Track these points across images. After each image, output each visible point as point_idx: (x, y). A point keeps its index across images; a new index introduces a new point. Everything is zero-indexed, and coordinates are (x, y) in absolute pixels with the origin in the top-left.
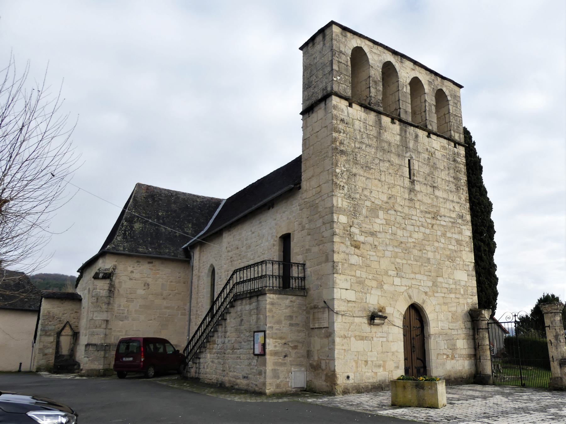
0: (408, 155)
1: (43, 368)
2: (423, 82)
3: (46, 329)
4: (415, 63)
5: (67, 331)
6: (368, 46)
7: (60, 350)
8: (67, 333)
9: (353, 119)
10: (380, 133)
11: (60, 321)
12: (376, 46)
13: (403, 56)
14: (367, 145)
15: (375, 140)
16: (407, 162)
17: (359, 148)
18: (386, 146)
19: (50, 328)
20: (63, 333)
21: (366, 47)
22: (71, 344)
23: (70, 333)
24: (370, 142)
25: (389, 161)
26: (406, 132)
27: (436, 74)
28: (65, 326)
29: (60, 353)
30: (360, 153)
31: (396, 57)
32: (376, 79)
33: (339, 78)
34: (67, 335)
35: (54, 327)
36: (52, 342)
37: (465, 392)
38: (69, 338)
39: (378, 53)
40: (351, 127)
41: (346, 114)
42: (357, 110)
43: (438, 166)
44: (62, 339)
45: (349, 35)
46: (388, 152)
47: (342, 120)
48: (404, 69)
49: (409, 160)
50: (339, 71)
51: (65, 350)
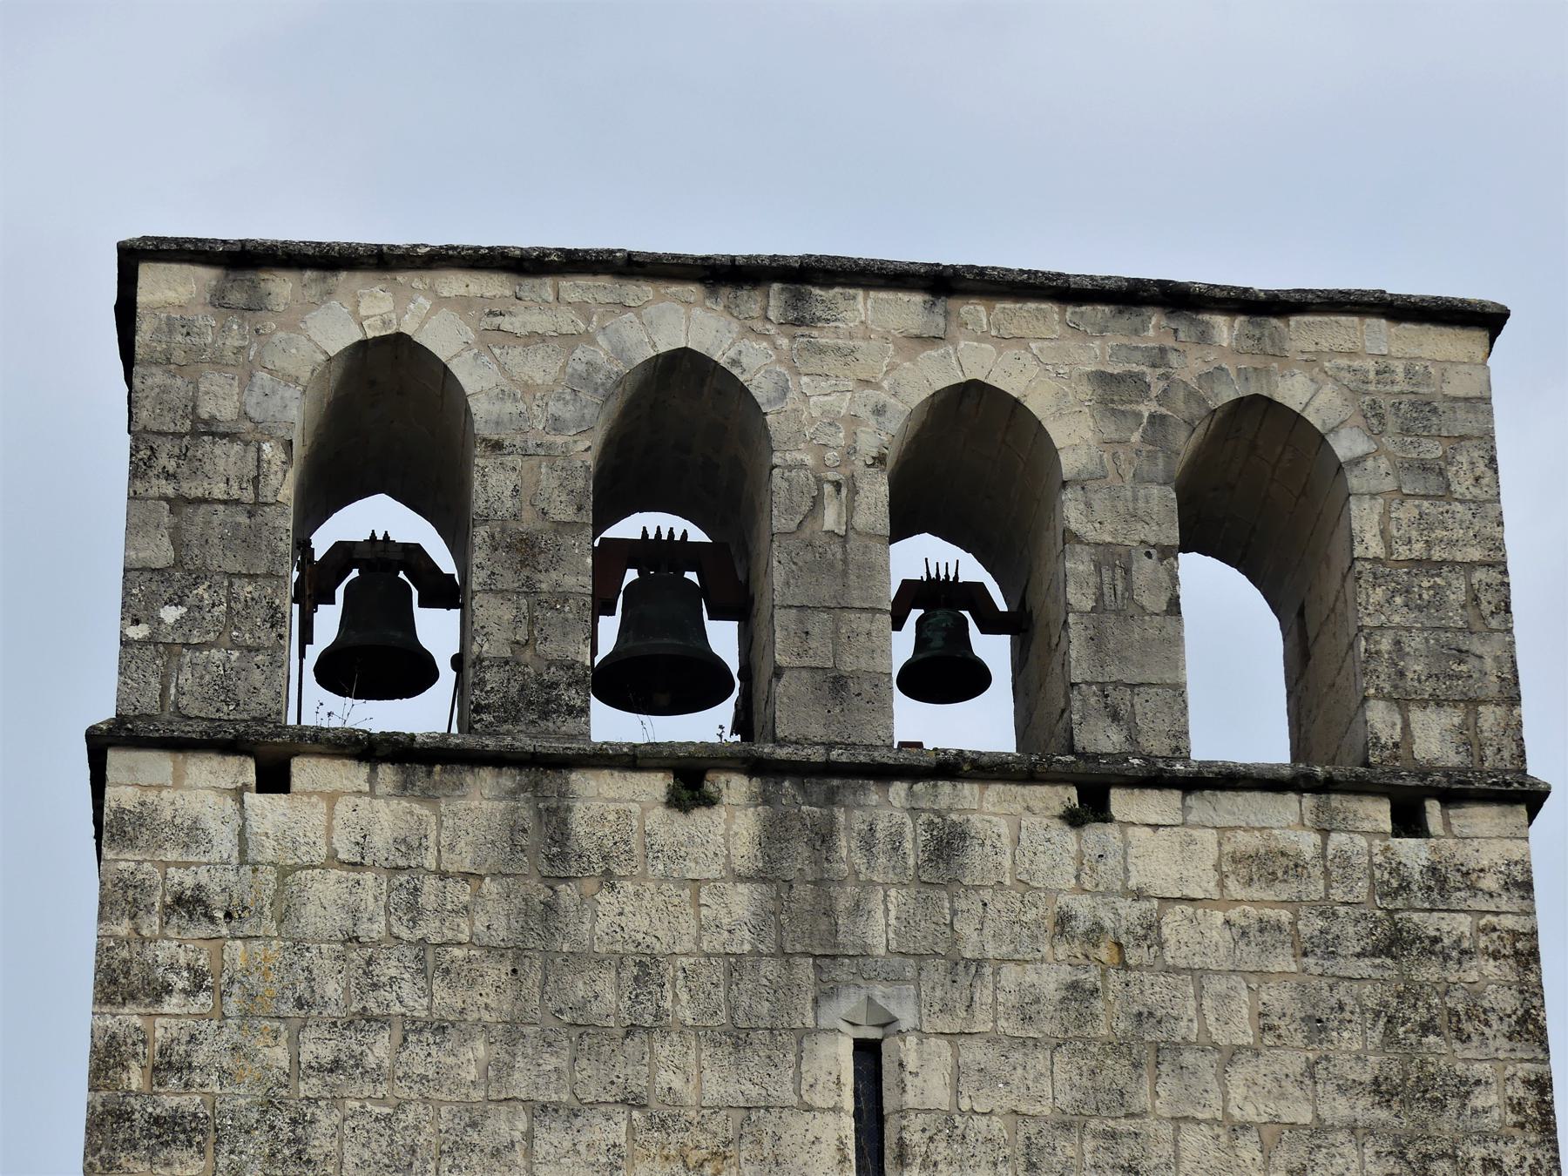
0: (848, 1004)
2: (1036, 405)
4: (942, 283)
6: (463, 304)
9: (284, 872)
10: (550, 907)
12: (545, 287)
13: (805, 277)
14: (413, 1027)
15: (497, 972)
16: (836, 1059)
17: (336, 1066)
18: (607, 995)
21: (433, 318)
24: (445, 998)
25: (633, 1102)
26: (824, 838)
27: (1179, 300)
30: (336, 1101)
31: (751, 302)
32: (529, 522)
33: (170, 614)
39: (566, 321)
40: (271, 927)
41: (225, 846)
42: (332, 798)
43: (1186, 1029)
45: (282, 286)
46: (630, 1031)
47: (189, 904)
48: (831, 363)
49: (868, 1053)
50: (179, 563)
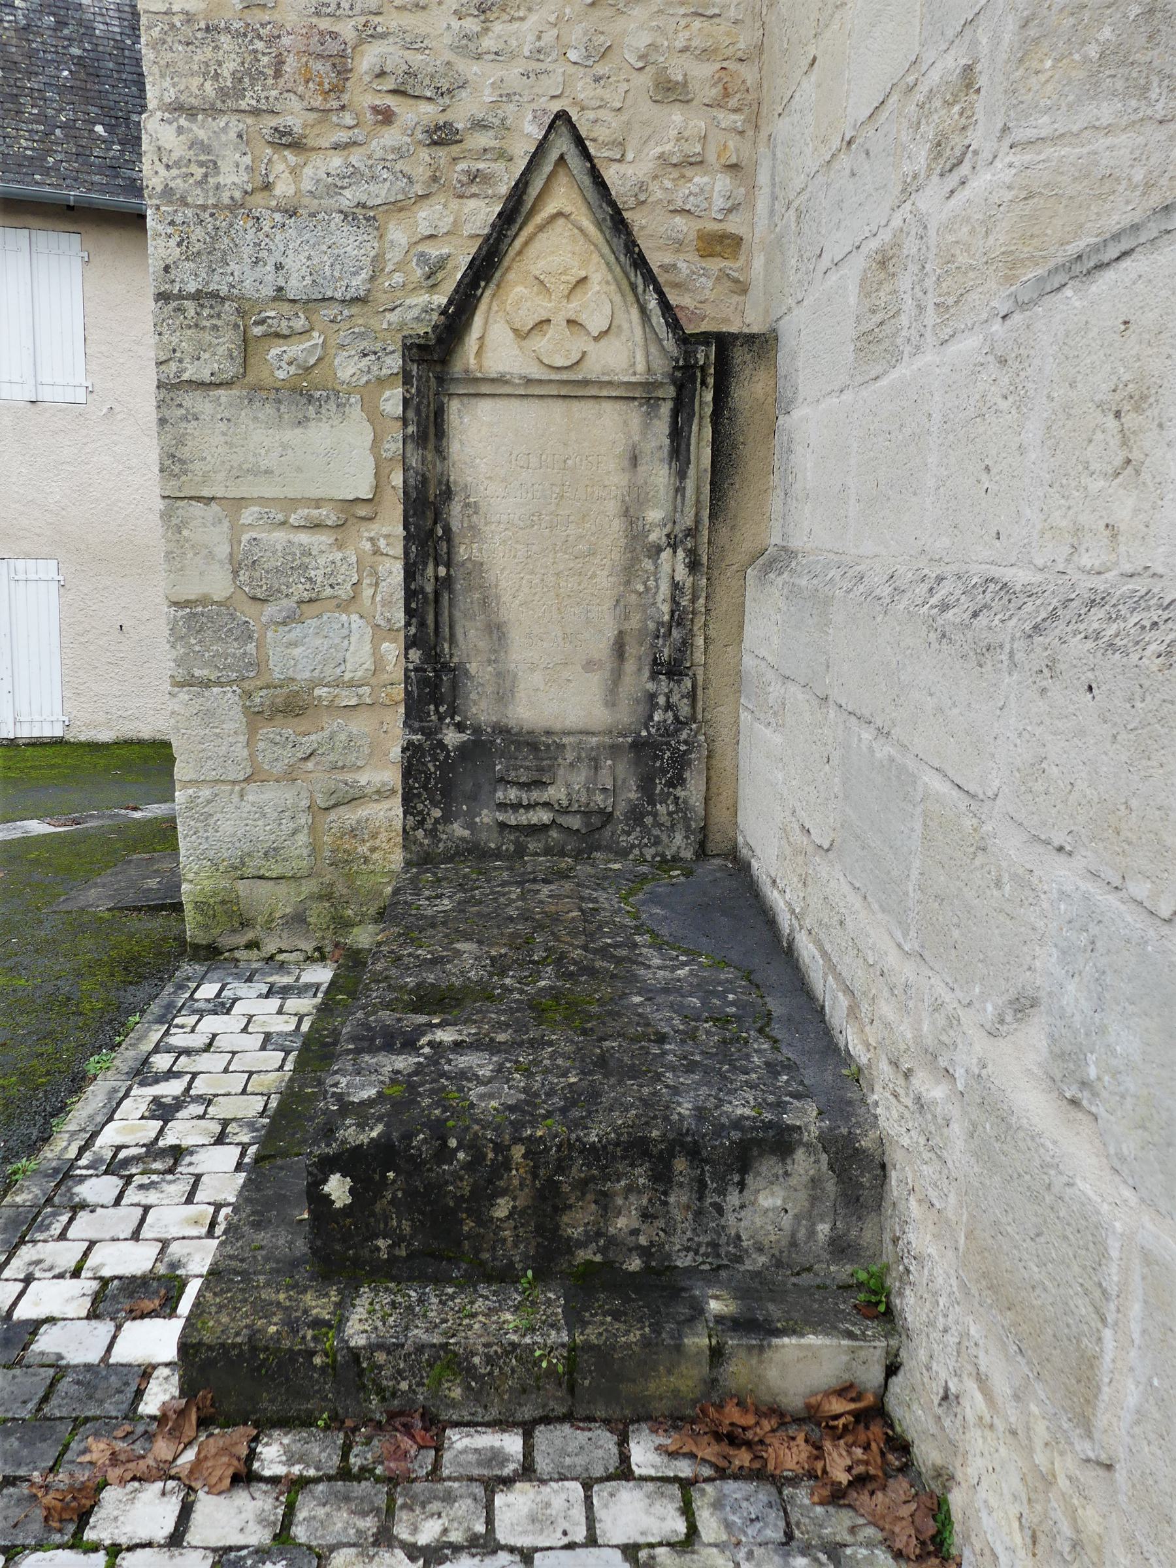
1: (278, 899)
3: (248, 277)
5: (561, 306)
7: (469, 644)
8: (556, 347)
11: (442, 136)
19: (301, 258)
20: (492, 344)
22: (639, 548)
23: (627, 350)
28: (513, 213)
29: (481, 709)
34: (572, 387)
35: (352, 244)
36: (353, 513)
37: (107, 822)
38: (611, 429)
44: (483, 439)
51: (552, 670)
